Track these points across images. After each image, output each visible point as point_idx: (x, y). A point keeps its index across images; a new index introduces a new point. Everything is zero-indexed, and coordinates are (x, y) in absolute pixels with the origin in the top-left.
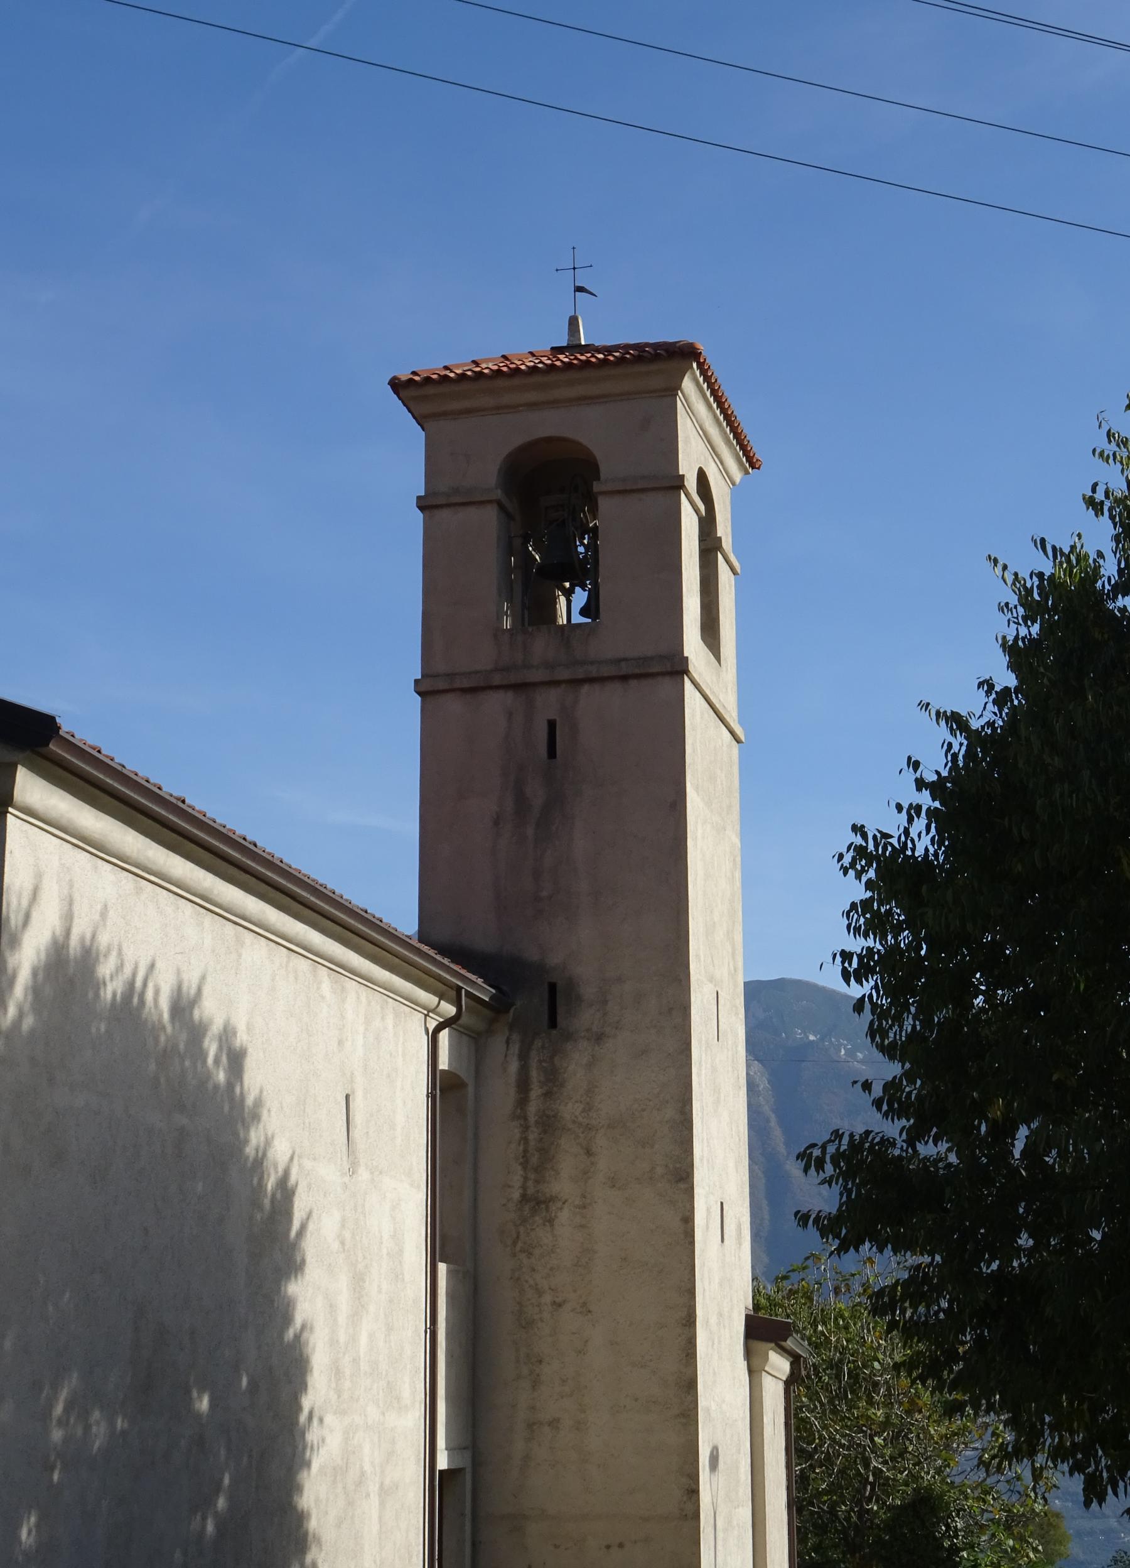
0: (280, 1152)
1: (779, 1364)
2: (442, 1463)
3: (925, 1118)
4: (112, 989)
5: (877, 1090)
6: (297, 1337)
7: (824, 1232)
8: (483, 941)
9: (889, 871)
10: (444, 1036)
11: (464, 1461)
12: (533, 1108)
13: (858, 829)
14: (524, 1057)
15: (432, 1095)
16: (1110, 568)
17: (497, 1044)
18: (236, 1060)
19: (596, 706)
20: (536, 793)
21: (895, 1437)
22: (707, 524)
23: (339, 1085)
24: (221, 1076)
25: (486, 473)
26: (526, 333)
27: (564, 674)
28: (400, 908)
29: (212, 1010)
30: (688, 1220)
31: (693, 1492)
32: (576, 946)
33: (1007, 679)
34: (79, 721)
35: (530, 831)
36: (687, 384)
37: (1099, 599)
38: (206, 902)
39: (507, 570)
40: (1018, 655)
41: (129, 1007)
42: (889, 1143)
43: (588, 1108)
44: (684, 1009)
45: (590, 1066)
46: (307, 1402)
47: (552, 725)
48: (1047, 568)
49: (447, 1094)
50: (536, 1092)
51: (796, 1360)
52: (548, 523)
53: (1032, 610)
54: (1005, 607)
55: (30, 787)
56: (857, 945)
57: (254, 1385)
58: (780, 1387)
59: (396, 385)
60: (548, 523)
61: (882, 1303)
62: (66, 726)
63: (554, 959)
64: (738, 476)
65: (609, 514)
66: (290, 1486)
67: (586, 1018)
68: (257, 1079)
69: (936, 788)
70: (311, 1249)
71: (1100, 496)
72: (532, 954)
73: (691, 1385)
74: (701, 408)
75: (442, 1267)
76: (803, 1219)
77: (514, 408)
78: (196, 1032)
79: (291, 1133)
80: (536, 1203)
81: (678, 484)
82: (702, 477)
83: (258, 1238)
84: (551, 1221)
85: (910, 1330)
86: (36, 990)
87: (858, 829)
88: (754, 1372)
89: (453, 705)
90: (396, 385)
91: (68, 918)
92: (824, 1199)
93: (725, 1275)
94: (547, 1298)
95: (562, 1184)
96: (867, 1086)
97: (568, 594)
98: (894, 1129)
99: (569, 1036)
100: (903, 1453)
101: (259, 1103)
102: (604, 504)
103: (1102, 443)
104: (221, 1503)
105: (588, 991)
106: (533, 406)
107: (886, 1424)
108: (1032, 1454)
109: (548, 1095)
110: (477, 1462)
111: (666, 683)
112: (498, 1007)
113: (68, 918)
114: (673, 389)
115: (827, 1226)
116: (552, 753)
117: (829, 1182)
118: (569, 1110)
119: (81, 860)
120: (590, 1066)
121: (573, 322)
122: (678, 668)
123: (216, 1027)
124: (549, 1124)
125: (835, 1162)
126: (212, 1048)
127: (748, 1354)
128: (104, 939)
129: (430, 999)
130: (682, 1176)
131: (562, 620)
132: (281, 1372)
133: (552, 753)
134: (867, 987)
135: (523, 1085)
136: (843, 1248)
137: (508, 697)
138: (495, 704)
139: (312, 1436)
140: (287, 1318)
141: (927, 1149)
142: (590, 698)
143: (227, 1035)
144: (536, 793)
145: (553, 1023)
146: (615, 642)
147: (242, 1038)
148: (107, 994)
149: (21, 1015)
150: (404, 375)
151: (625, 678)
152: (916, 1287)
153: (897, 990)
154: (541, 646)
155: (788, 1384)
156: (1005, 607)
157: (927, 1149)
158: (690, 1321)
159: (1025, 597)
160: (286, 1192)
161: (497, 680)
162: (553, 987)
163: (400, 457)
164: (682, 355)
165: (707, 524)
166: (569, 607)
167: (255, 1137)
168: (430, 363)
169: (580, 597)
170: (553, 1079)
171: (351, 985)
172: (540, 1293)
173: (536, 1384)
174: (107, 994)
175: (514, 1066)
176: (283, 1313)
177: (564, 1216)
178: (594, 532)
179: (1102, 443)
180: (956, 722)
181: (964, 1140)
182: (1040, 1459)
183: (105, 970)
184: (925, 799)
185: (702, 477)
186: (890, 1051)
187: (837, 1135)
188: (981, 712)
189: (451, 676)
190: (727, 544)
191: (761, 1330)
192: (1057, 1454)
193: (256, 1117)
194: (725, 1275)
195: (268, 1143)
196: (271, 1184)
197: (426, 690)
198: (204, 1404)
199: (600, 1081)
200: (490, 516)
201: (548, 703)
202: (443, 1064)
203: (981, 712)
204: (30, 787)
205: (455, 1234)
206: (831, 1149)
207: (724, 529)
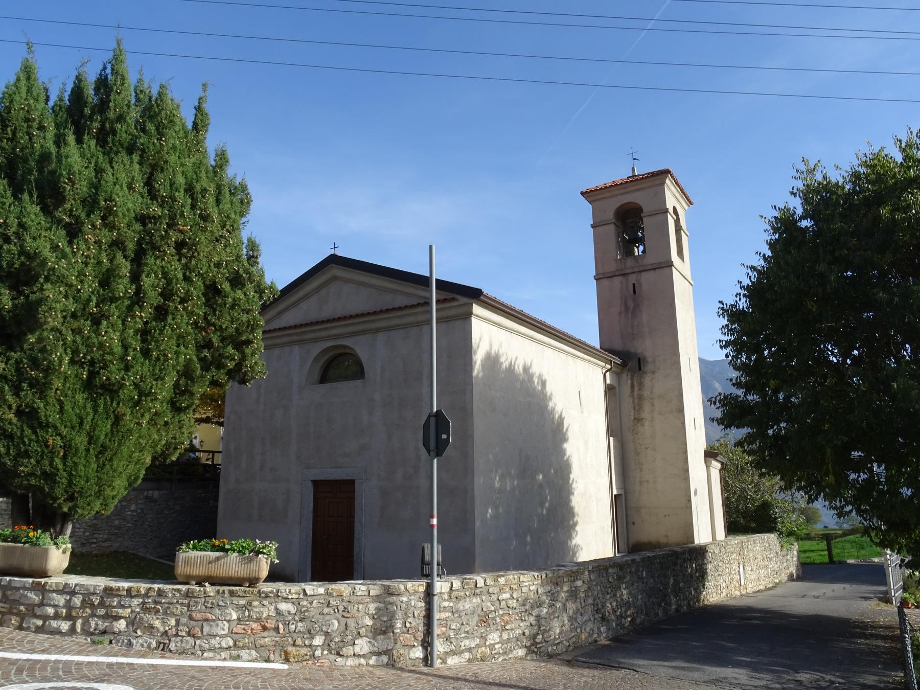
0: (558, 409)
1: (716, 465)
2: (615, 492)
3: (749, 388)
4: (505, 365)
5: (734, 381)
6: (567, 460)
7: (719, 424)
8: (618, 346)
9: (733, 314)
10: (608, 374)
11: (622, 492)
12: (636, 393)
13: (720, 302)
14: (632, 379)
15: (605, 391)
16: (800, 211)
17: (624, 376)
18: (544, 383)
19: (647, 279)
20: (631, 304)
21: (756, 486)
22: (677, 222)
23: (577, 391)
24: (539, 388)
25: (610, 215)
26: (621, 174)
27: (636, 270)
28: (595, 341)
29: (535, 370)
30: (684, 423)
31: (690, 501)
32: (645, 347)
33: (769, 253)
34: (489, 290)
35: (630, 315)
36: (667, 181)
37: (795, 222)
38: (532, 339)
39: (618, 242)
40: (772, 245)
41: (511, 369)
42: (737, 396)
43: (652, 393)
44: (678, 363)
45: (651, 381)
46: (572, 476)
47: (634, 285)
48: (777, 214)
49: (610, 390)
50: (636, 389)
51: (722, 463)
52: (629, 225)
53: (775, 230)
54: (766, 231)
55: (477, 309)
56: (726, 338)
57: (556, 472)
58: (718, 472)
59: (582, 193)
60: (629, 225)
61: (739, 444)
62: (485, 291)
63: (639, 351)
64: (686, 207)
65: (647, 222)
66: (568, 501)
67: (650, 367)
68: (549, 389)
69: (747, 288)
70: (571, 435)
71: (795, 191)
72: (633, 350)
73: (687, 470)
74: (672, 188)
75: (611, 439)
76: (713, 420)
77: (616, 195)
78: (531, 377)
79: (561, 401)
80: (638, 420)
81: (667, 211)
82: (675, 209)
83: (555, 433)
84: (643, 425)
85: (750, 453)
86: (483, 365)
87: (720, 302)
88: (708, 467)
89: (605, 282)
90: (582, 193)
91: (491, 345)
92: (718, 414)
93: (696, 437)
94: (643, 447)
95: (646, 414)
96: (731, 380)
97: (638, 247)
98: (740, 392)
99: (645, 373)
100: (759, 490)
101: (551, 394)
102: (645, 220)
103: (795, 174)
104: (547, 504)
105: (650, 360)
106: (622, 194)
107: (752, 481)
108: (791, 488)
109: (640, 389)
110: (625, 493)
111: (667, 270)
112: (624, 365)
113: (491, 345)
114: (663, 183)
115: (720, 422)
116: (635, 293)
117: (718, 408)
118: (646, 393)
119: (495, 329)
120: (651, 381)
121: (633, 169)
122: (670, 265)
123: (537, 375)
124: (640, 397)
125: (720, 401)
126: (536, 381)
127: (706, 462)
128: (501, 352)
129: (603, 364)
130: (681, 410)
131: (636, 254)
132: (564, 469)
133: (635, 293)
134: (728, 350)
135: (632, 387)
136: (726, 428)
137: (621, 278)
138: (617, 281)
139: (574, 486)
140: (565, 454)
141: (750, 398)
142: (645, 276)
143: (540, 377)
144: (631, 304)
145: (640, 369)
146: (650, 260)
147: (545, 377)
148: (504, 366)
149: (478, 372)
150: (584, 190)
151: (654, 269)
152: (750, 439)
153: (738, 352)
154: (630, 262)
155: (720, 470)
156: (766, 231)
157: (750, 398)
158: (686, 452)
159: (773, 228)
160: (561, 419)
161: (617, 273)
162: (639, 359)
163: (585, 211)
164: (666, 172)
165: (677, 222)
166: (638, 251)
167: (551, 404)
168: (592, 186)
169: (641, 248)
170: (641, 385)
171: (578, 361)
172: (641, 445)
173: (641, 471)
174: (504, 366)
175: (629, 382)
176: (562, 452)
177: (647, 423)
178: (643, 229)
179: (795, 174)
180: (753, 268)
181: (763, 395)
182: (793, 490)
183: (502, 360)
184: (743, 292)
185: (675, 209)
186: (736, 368)
187: (720, 394)
188: (759, 263)
189: (604, 274)
190: (684, 227)
191: (710, 454)
192: (799, 489)
193: (550, 398)
194: (696, 437)
195: (555, 405)
196: (557, 416)
197: (597, 278)
198: (541, 477)
199: (654, 384)
200: (612, 227)
201: (632, 279)
202: (608, 382)
203: (759, 263)
204: (477, 309)
205: (615, 429)
206: (718, 398)
207: (683, 223)
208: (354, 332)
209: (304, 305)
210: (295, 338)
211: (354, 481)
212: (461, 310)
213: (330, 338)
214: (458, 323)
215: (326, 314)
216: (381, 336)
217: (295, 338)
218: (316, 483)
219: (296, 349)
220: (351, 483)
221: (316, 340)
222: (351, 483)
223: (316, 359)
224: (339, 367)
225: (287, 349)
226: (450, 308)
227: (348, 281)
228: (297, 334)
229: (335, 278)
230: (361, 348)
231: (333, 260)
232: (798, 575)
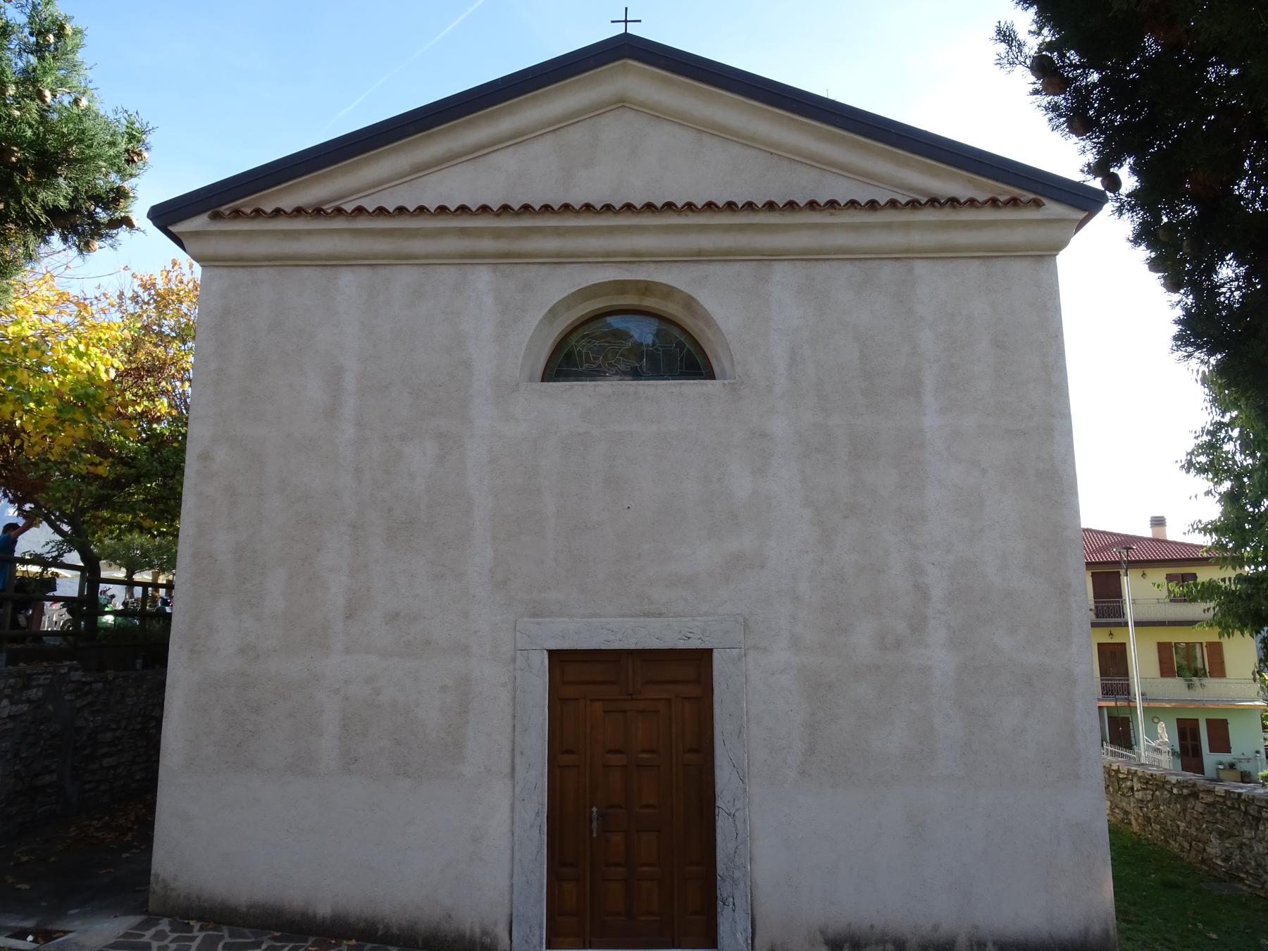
208: (699, 253)
209: (506, 161)
210: (488, 245)
211: (710, 651)
212: (1040, 235)
213: (608, 258)
214: (1019, 268)
215: (593, 186)
216: (782, 273)
217: (488, 245)
218: (558, 658)
219: (482, 277)
220: (701, 660)
221: (560, 260)
222: (701, 660)
223: (553, 313)
224: (631, 342)
225: (448, 275)
226: (1010, 224)
227: (659, 115)
228: (498, 234)
229: (621, 103)
230: (721, 302)
231: (626, 49)
232: (135, 911)
